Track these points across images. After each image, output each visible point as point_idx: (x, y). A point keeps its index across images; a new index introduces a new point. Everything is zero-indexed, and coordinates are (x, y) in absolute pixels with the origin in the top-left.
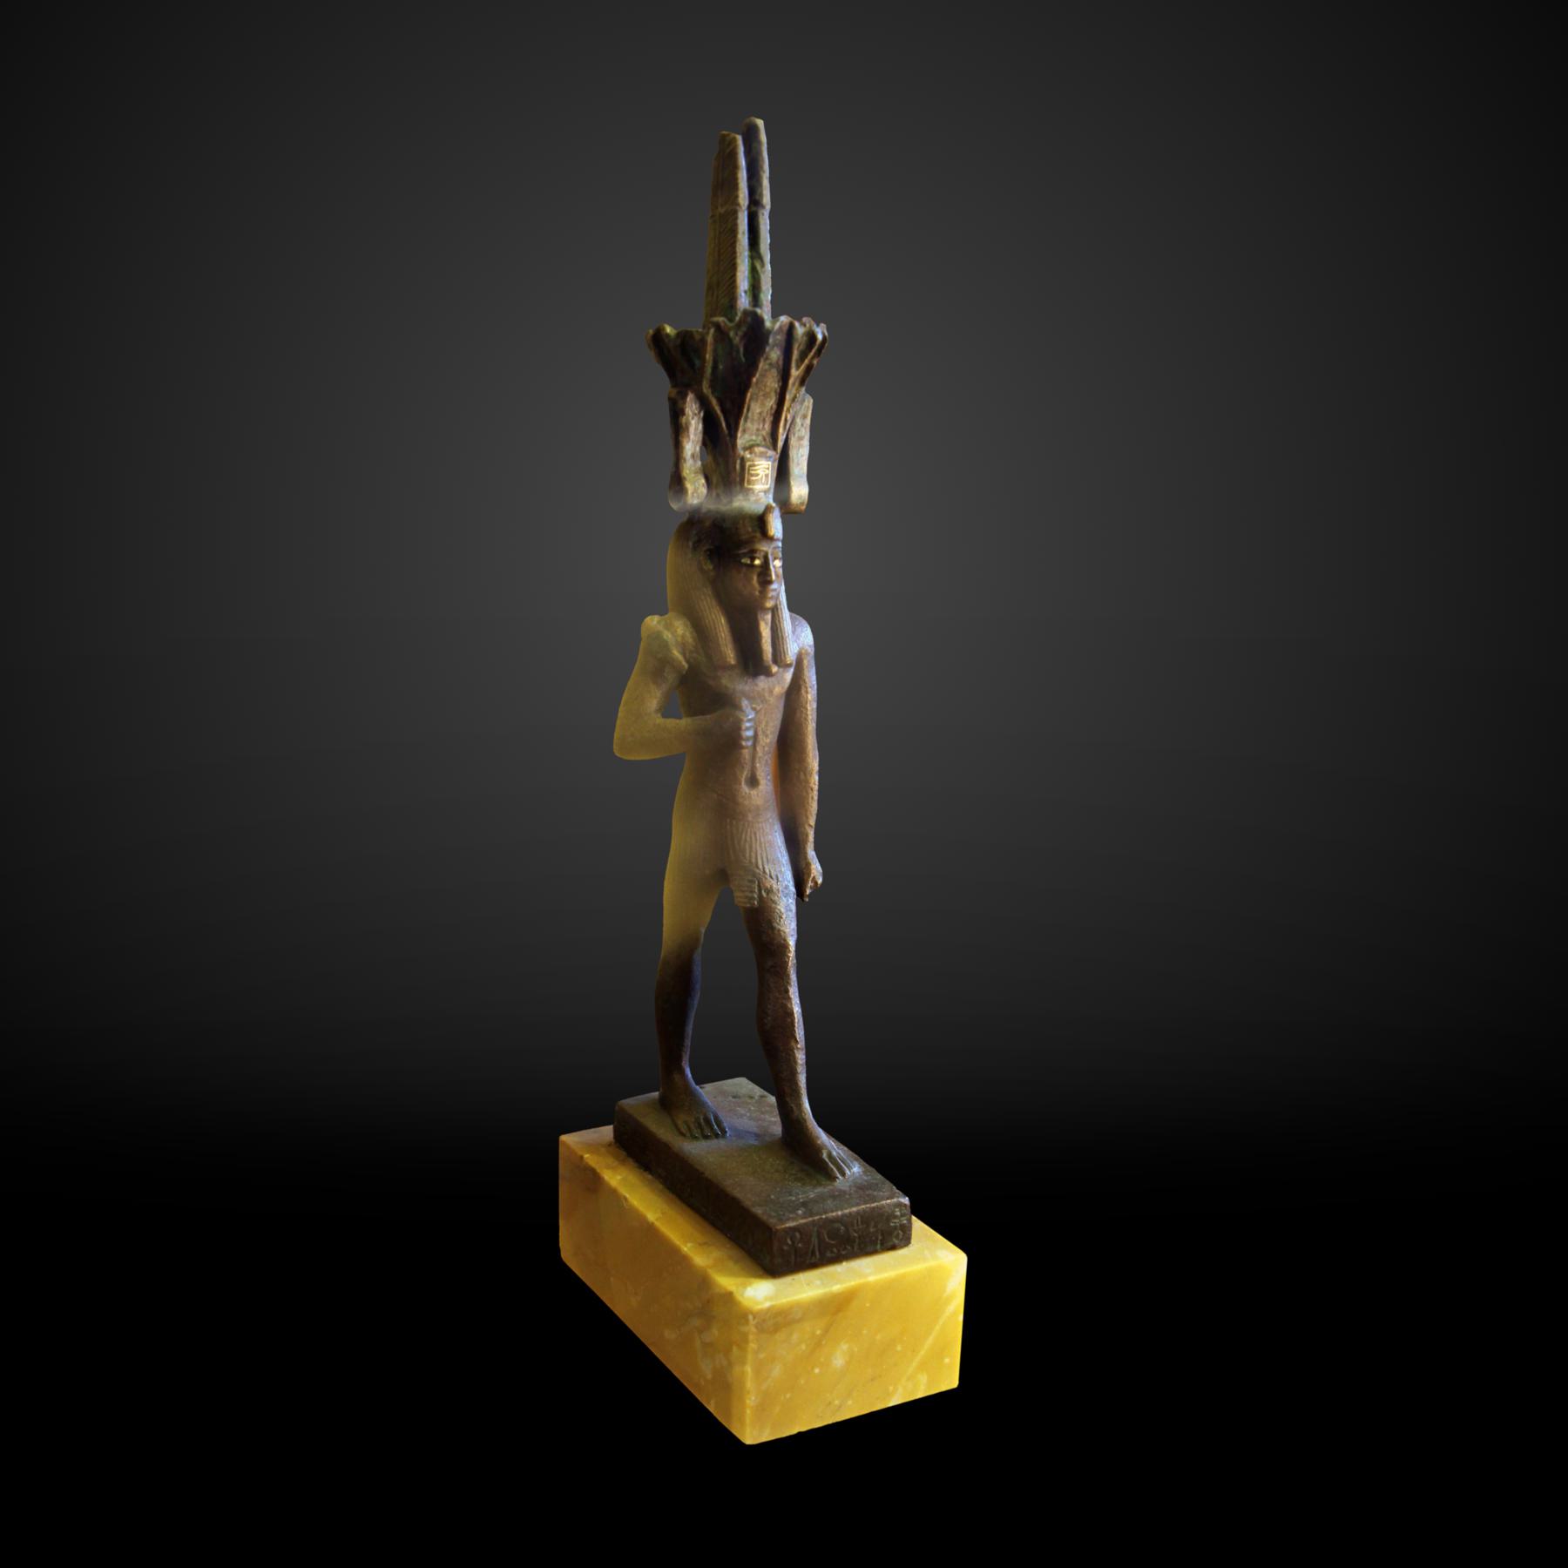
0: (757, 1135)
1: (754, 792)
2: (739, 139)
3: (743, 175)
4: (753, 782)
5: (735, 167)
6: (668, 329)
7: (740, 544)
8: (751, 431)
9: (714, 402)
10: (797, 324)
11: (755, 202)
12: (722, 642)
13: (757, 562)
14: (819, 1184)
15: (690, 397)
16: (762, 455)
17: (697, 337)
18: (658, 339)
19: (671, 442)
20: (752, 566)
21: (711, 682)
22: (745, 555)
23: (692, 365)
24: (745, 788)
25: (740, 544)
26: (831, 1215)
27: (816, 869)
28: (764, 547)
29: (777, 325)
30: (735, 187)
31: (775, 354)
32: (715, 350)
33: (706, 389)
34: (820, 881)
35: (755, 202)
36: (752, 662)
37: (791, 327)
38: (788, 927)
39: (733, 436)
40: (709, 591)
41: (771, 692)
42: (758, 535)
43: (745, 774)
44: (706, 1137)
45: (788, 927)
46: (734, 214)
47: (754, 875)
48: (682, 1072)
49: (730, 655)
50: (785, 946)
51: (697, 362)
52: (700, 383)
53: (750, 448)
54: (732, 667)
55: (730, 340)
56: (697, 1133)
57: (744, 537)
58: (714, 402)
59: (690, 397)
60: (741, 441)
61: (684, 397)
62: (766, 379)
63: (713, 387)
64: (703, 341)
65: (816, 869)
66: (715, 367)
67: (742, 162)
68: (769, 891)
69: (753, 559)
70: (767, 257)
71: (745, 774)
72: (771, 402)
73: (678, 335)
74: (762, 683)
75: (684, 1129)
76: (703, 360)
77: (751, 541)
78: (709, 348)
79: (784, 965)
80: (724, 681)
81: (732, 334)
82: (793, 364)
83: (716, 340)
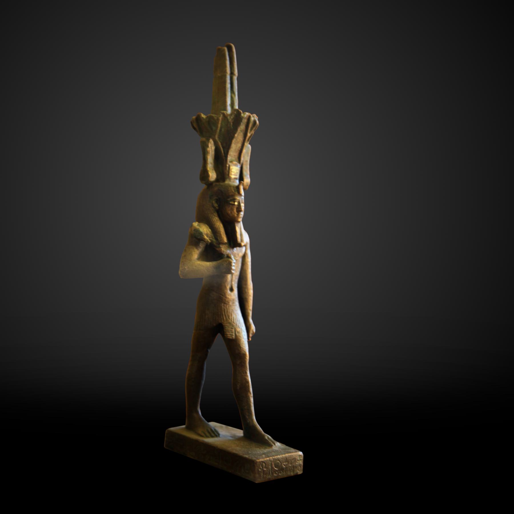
0: (232, 437)
1: (232, 294)
2: (226, 49)
3: (228, 63)
4: (232, 290)
5: (225, 59)
6: (203, 116)
7: (228, 197)
8: (232, 154)
9: (220, 143)
10: (251, 116)
11: (232, 74)
12: (222, 233)
13: (236, 203)
14: (265, 448)
15: (211, 141)
16: (236, 165)
17: (216, 118)
18: (198, 119)
19: (202, 156)
20: (234, 205)
21: (217, 249)
22: (231, 200)
23: (212, 129)
24: (229, 292)
25: (228, 197)
26: (276, 457)
27: (253, 328)
28: (238, 198)
29: (245, 116)
30: (225, 66)
31: (242, 127)
32: (221, 124)
33: (217, 138)
34: (255, 331)
35: (232, 74)
36: (234, 243)
37: (249, 118)
38: (246, 347)
39: (226, 157)
40: (216, 214)
41: (238, 255)
42: (236, 193)
43: (228, 287)
44: (212, 437)
45: (246, 347)
46: (225, 76)
47: (233, 326)
48: (198, 412)
49: (225, 240)
50: (245, 355)
51: (214, 128)
52: (215, 136)
53: (231, 162)
54: (225, 244)
55: (228, 120)
56: (208, 434)
57: (230, 194)
58: (220, 143)
59: (211, 141)
60: (229, 158)
61: (208, 140)
62: (239, 136)
63: (219, 138)
64: (218, 119)
65: (253, 328)
66: (221, 130)
67: (228, 58)
68: (239, 332)
69: (234, 202)
70: (236, 93)
71: (228, 287)
72: (239, 145)
73: (207, 117)
74: (236, 250)
75: (203, 434)
76: (217, 127)
77: (233, 196)
78: (220, 122)
79: (245, 362)
80: (223, 249)
81: (229, 117)
82: (249, 131)
83: (222, 119)
